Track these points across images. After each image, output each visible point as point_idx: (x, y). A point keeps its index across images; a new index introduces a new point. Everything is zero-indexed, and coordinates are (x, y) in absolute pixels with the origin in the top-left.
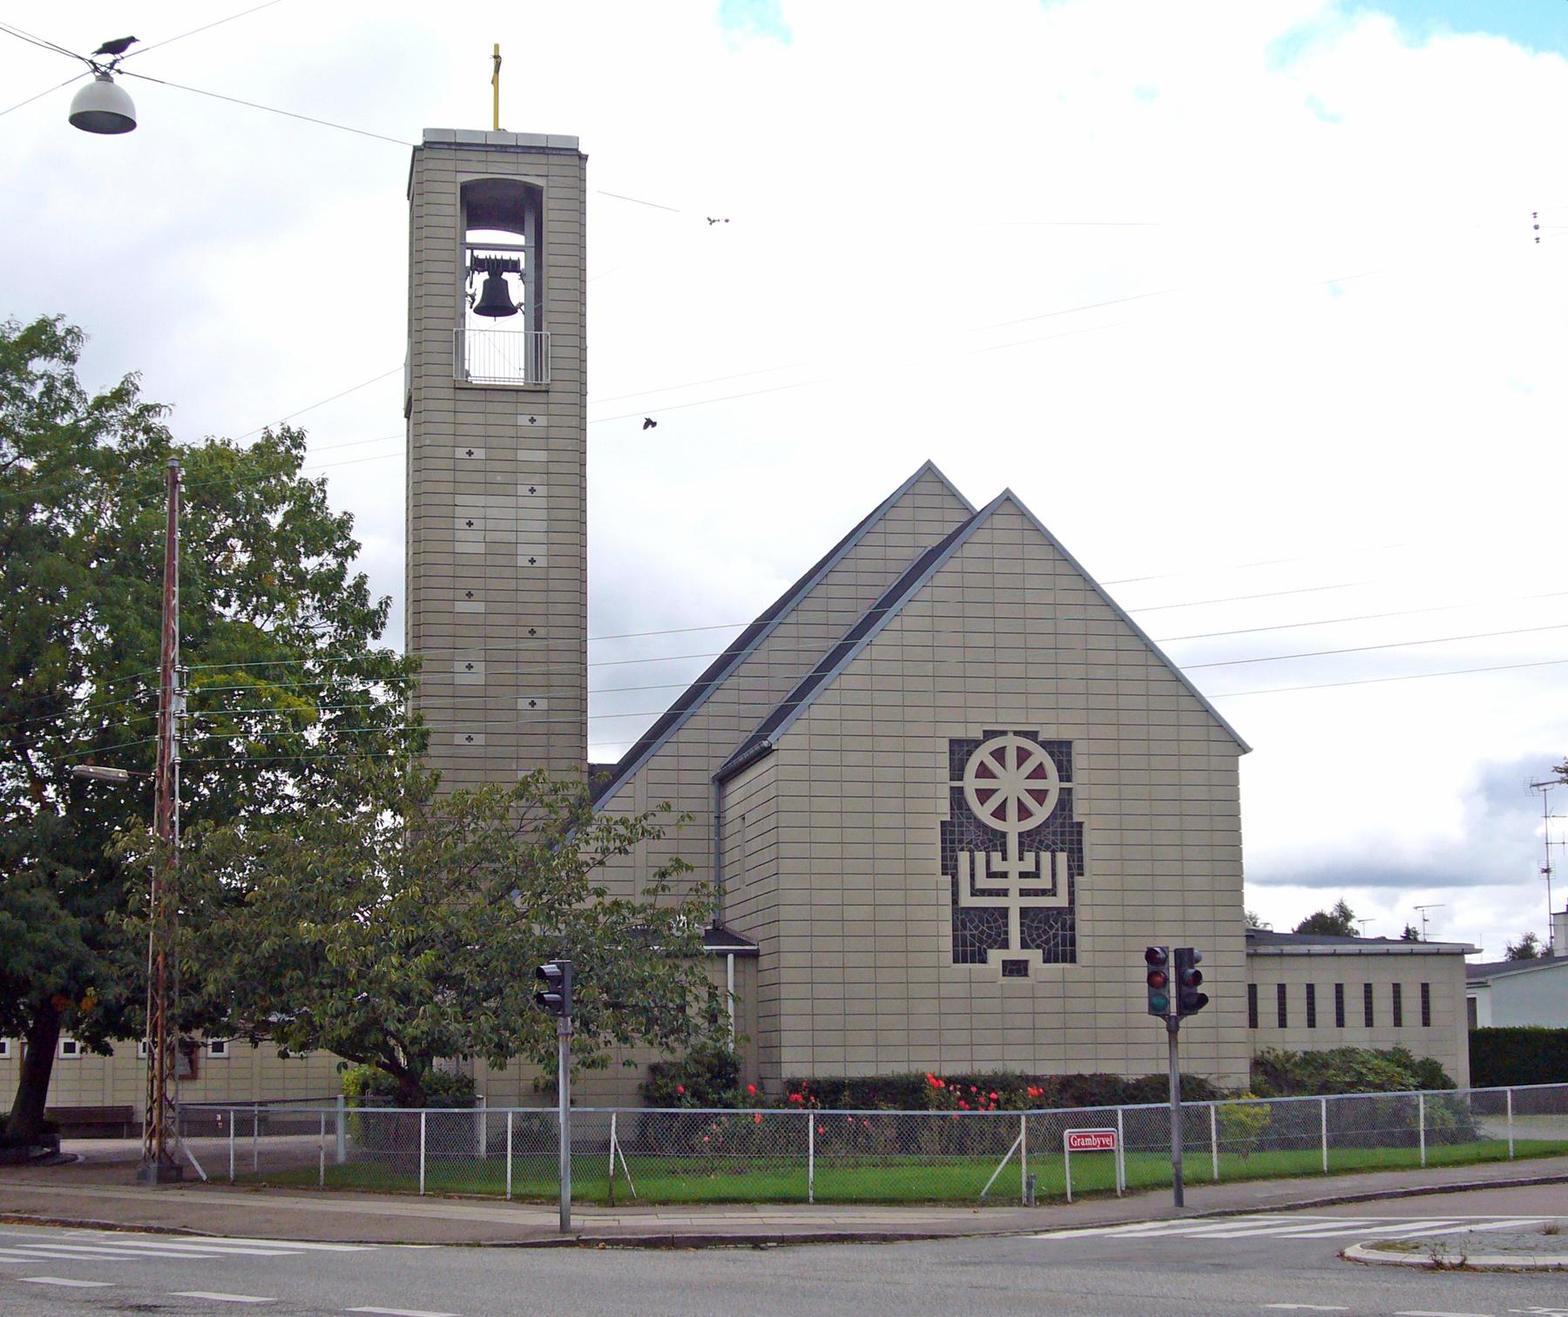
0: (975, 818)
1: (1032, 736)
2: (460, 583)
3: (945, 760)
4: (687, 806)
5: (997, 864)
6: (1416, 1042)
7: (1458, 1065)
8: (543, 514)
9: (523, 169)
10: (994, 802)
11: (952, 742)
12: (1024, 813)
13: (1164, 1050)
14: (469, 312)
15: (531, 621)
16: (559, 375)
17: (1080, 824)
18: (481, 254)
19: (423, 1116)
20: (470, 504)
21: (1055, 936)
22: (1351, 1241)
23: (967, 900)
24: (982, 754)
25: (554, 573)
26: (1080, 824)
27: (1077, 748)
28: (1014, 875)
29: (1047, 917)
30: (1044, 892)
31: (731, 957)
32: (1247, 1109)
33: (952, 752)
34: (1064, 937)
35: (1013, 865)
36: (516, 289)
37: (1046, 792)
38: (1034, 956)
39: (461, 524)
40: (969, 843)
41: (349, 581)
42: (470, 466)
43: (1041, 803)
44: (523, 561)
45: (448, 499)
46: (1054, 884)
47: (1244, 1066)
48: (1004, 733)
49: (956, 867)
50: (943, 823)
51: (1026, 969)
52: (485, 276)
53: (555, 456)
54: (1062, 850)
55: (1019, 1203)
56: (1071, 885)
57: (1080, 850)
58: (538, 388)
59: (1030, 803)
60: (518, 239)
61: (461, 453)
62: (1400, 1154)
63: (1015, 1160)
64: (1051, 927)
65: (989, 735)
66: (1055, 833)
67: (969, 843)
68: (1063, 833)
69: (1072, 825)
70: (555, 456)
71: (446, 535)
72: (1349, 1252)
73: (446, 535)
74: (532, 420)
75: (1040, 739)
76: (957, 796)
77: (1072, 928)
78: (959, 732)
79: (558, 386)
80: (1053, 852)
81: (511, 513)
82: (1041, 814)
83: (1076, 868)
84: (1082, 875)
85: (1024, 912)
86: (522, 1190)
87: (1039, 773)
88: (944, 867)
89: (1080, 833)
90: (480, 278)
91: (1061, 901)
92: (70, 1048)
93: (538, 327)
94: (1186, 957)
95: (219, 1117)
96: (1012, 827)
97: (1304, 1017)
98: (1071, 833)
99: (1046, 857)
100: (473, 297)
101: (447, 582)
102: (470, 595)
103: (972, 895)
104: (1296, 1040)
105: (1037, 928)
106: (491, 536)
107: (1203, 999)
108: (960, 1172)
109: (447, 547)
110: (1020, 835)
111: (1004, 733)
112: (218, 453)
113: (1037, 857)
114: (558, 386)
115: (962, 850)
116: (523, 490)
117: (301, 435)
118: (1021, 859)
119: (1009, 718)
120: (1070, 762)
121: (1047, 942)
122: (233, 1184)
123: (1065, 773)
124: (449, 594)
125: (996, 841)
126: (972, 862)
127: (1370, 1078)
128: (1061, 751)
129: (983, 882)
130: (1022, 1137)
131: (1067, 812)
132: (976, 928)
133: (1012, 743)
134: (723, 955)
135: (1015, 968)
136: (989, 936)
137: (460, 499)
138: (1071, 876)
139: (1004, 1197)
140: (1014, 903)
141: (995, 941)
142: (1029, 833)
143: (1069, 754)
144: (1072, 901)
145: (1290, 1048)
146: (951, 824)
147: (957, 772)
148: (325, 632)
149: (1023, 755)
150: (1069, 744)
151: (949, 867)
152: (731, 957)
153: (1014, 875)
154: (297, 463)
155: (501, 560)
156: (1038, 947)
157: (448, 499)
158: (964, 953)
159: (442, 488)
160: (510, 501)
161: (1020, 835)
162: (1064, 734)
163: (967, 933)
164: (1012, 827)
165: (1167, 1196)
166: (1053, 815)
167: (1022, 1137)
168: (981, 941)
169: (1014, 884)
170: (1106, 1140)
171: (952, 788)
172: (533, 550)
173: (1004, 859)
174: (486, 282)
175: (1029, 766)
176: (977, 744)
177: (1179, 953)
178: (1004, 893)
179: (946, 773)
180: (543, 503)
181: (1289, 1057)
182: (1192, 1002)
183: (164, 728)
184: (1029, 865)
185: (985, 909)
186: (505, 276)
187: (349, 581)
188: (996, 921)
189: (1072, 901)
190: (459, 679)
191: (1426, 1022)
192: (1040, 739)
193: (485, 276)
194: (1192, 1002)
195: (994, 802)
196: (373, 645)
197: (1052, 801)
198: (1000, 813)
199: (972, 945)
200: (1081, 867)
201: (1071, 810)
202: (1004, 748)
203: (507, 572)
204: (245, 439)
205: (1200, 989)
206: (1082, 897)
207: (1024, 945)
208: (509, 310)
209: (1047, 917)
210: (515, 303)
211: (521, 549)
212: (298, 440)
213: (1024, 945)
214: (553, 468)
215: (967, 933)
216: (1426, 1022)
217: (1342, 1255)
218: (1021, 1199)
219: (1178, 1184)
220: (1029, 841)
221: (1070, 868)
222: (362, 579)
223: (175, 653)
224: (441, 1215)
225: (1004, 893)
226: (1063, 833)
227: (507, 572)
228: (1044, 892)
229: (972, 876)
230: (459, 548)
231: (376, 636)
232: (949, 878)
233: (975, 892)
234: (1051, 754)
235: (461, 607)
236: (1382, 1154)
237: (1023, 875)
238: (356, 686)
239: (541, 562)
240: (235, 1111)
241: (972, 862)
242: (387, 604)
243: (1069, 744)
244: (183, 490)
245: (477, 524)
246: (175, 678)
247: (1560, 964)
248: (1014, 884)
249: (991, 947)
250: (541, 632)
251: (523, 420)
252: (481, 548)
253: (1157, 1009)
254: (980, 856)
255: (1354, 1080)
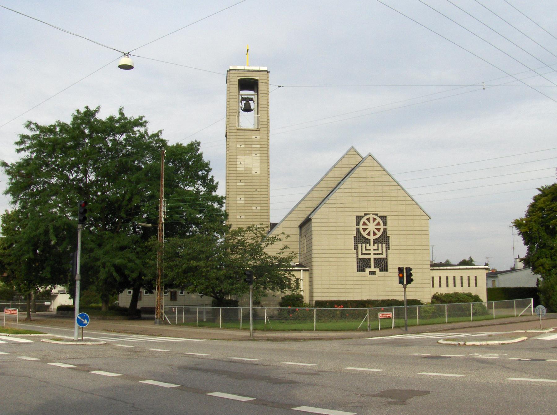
0: (363, 235)
1: (377, 215)
2: (238, 178)
3: (355, 221)
4: (289, 233)
5: (368, 247)
6: (473, 291)
7: (484, 297)
8: (259, 161)
9: (254, 75)
10: (367, 232)
11: (357, 216)
12: (375, 234)
13: (403, 293)
14: (241, 111)
15: (256, 187)
16: (262, 126)
17: (389, 237)
18: (244, 97)
19: (221, 309)
20: (241, 158)
21: (383, 265)
22: (440, 339)
23: (360, 256)
24: (364, 220)
25: (262, 175)
26: (389, 237)
27: (388, 218)
28: (372, 250)
29: (380, 260)
30: (380, 254)
31: (302, 270)
32: (429, 307)
33: (356, 219)
34: (385, 265)
35: (372, 247)
36: (253, 105)
37: (380, 229)
38: (377, 270)
39: (238, 163)
40: (361, 242)
41: (209, 177)
42: (241, 149)
43: (379, 232)
44: (254, 172)
45: (235, 157)
46: (382, 252)
47: (431, 297)
48: (370, 214)
49: (357, 248)
50: (354, 237)
51: (375, 273)
52: (245, 102)
53: (262, 146)
54: (384, 243)
55: (367, 330)
56: (387, 252)
57: (389, 243)
58: (257, 129)
59: (376, 231)
60: (253, 93)
61: (238, 146)
62: (465, 318)
63: (366, 321)
64: (382, 263)
65: (365, 214)
66: (382, 239)
67: (361, 242)
68: (384, 239)
69: (386, 237)
70: (262, 146)
71: (235, 166)
72: (439, 342)
73: (235, 166)
74: (256, 137)
75: (379, 215)
76: (358, 231)
77: (387, 263)
78: (359, 214)
79: (262, 129)
80: (382, 244)
81: (251, 161)
82: (379, 234)
83: (388, 248)
84: (389, 249)
85: (375, 259)
86: (244, 327)
87: (378, 224)
88: (355, 248)
89: (389, 239)
90: (244, 102)
91: (384, 256)
92: (130, 292)
93: (258, 114)
94: (409, 270)
95: (173, 309)
96: (372, 238)
97: (460, 284)
98: (386, 239)
99: (380, 245)
100: (242, 108)
101: (235, 178)
102: (241, 181)
103: (362, 255)
104: (444, 290)
105: (378, 263)
106: (246, 166)
107: (412, 280)
108: (353, 324)
109: (235, 169)
110: (374, 240)
111: (370, 214)
112: (179, 146)
113: (378, 245)
114: (262, 129)
115: (359, 243)
116: (254, 155)
117: (200, 143)
118: (374, 246)
119: (371, 210)
120: (386, 221)
121: (381, 266)
122: (177, 325)
123: (385, 223)
124: (235, 181)
125: (367, 241)
126: (362, 246)
127: (461, 299)
128: (384, 218)
129: (364, 252)
130: (368, 314)
131: (385, 234)
132: (363, 263)
133: (371, 217)
134: (300, 270)
135: (372, 273)
136: (366, 265)
137: (238, 157)
138: (387, 250)
139: (364, 329)
140: (372, 257)
141: (367, 266)
142: (376, 239)
143: (386, 219)
144: (387, 256)
145: (442, 292)
146: (356, 237)
147: (358, 223)
148: (203, 190)
149: (374, 220)
150: (386, 217)
151: (356, 248)
152: (302, 270)
153: (372, 250)
154: (198, 150)
155: (248, 172)
156: (378, 268)
157: (235, 157)
158: (360, 269)
159: (233, 154)
160: (251, 157)
161: (374, 240)
162: (384, 214)
163: (360, 264)
164: (372, 238)
165: (404, 329)
166: (382, 235)
167: (368, 314)
168: (364, 266)
169: (372, 252)
170: (389, 315)
171: (357, 228)
172: (256, 170)
173: (370, 246)
174: (245, 103)
175: (376, 222)
176: (363, 217)
177: (406, 268)
178: (370, 254)
179: (355, 224)
180: (259, 158)
181: (441, 295)
182: (410, 281)
183: (160, 215)
184: (376, 247)
185: (365, 258)
186: (250, 102)
187: (209, 177)
188: (368, 261)
189: (387, 256)
190: (238, 202)
191: (476, 286)
192: (379, 215)
193: (245, 102)
194: (410, 281)
195: (367, 232)
196: (214, 194)
197: (382, 231)
198: (369, 234)
199: (362, 267)
200: (389, 248)
201: (386, 233)
202: (370, 218)
203: (250, 175)
204: (185, 144)
205: (412, 277)
206: (389, 255)
207: (375, 267)
208: (251, 110)
209: (380, 260)
210: (252, 108)
211: (253, 169)
212: (199, 144)
213: (375, 267)
214: (261, 149)
215: (360, 264)
216: (476, 286)
217: (438, 342)
218: (367, 330)
219: (406, 326)
220: (376, 241)
221: (386, 248)
222: (213, 177)
223: (163, 196)
224: (223, 333)
225: (370, 254)
226: (384, 239)
227: (250, 175)
228: (380, 254)
229: (362, 250)
230: (238, 169)
231: (215, 192)
232: (356, 251)
233: (363, 254)
234: (382, 219)
235: (238, 184)
236: (461, 319)
237: (374, 250)
238: (210, 203)
239: (258, 173)
240: (177, 308)
241: (362, 246)
242: (218, 184)
243: (386, 217)
244: (165, 156)
245: (242, 163)
246: (163, 202)
247: (442, 268)
248: (372, 252)
249: (366, 268)
250: (258, 190)
251: (254, 137)
252: (243, 169)
253: (401, 282)
254: (364, 245)
255: (457, 300)
